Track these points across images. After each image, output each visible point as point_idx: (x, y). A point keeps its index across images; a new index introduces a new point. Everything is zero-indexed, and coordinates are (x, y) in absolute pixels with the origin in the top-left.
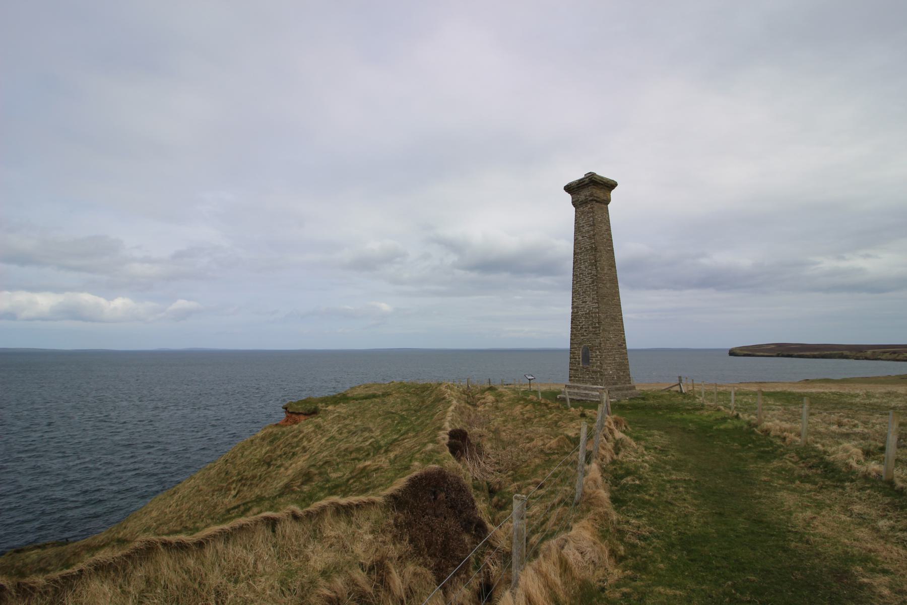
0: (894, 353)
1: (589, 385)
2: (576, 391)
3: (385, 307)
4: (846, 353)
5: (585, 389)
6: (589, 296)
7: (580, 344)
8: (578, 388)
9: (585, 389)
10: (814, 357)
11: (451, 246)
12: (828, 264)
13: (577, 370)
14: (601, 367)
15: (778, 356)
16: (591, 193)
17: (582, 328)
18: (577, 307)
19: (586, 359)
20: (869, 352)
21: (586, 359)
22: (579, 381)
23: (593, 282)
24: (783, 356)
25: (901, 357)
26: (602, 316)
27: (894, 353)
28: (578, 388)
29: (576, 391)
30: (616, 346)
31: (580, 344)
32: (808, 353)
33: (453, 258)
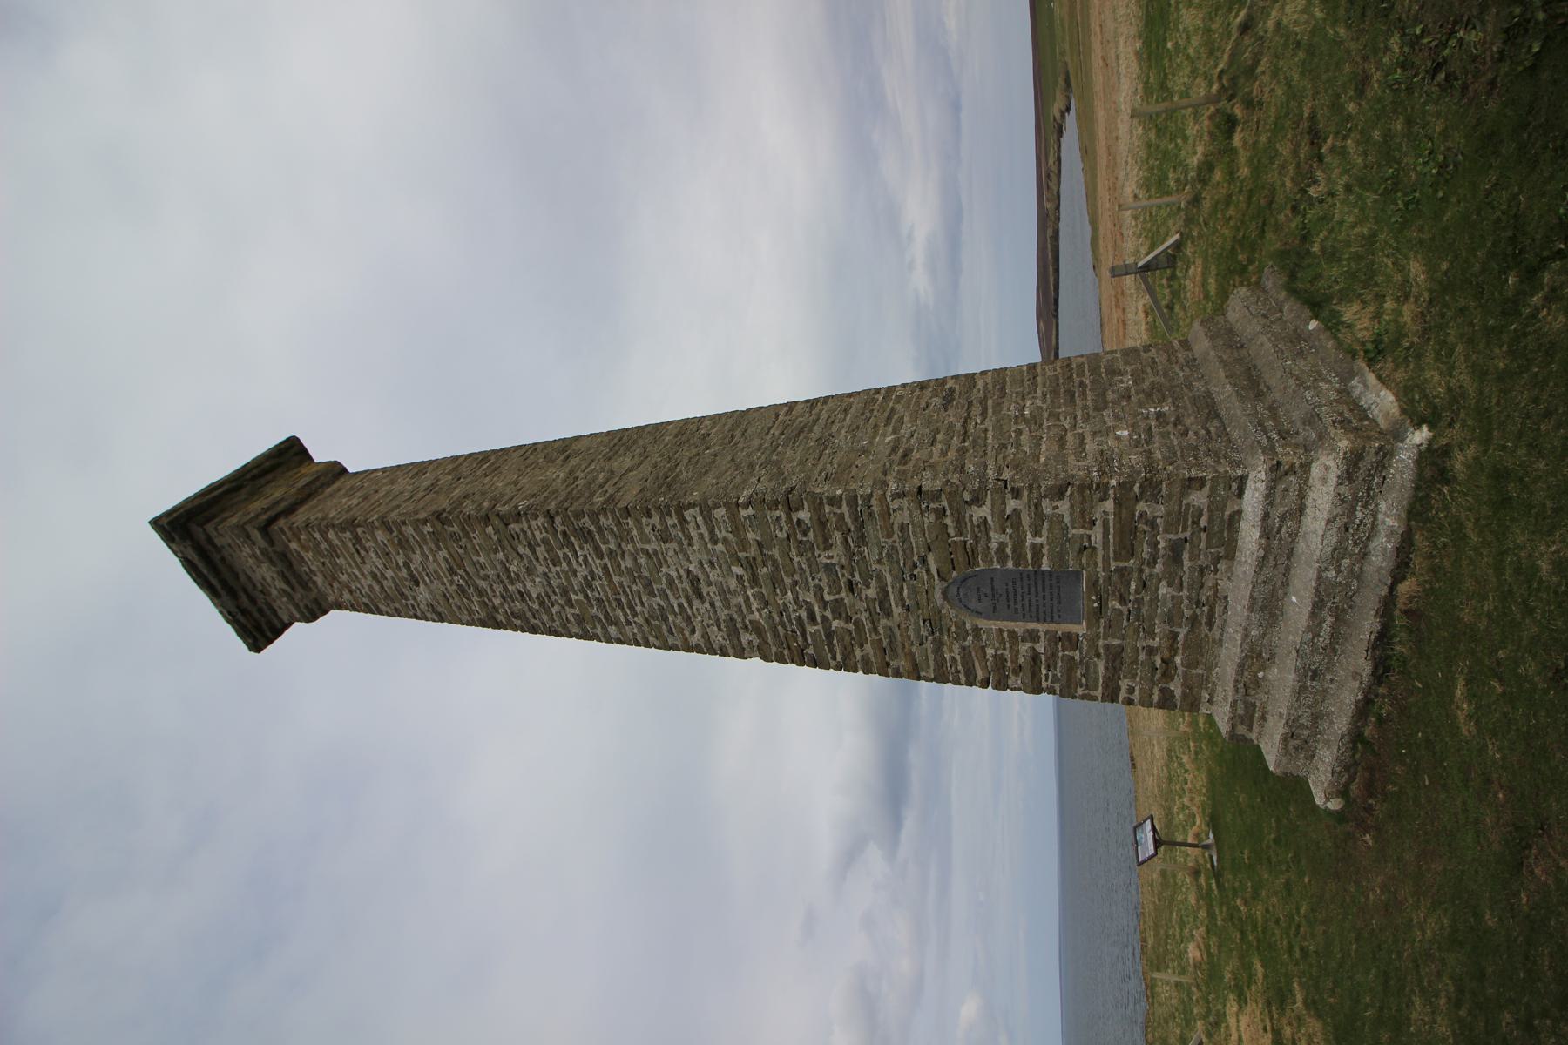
0: (1048, 176)
1: (1239, 583)
2: (1282, 678)
3: (969, 1009)
4: (1050, 232)
5: (1268, 607)
6: (657, 560)
7: (935, 623)
8: (1256, 657)
9: (1268, 607)
10: (1057, 271)
11: (850, 857)
12: (920, 281)
13: (1115, 658)
14: (1092, 490)
15: (1057, 317)
16: (263, 543)
17: (838, 609)
18: (733, 633)
19: (1038, 591)
20: (1048, 205)
21: (1038, 591)
22: (1200, 652)
23: (586, 536)
24: (1056, 310)
25: (1054, 169)
26: (762, 483)
27: (1048, 176)
28: (1256, 657)
29: (1282, 678)
30: (953, 417)
31: (935, 623)
32: (1051, 279)
33: (874, 855)
